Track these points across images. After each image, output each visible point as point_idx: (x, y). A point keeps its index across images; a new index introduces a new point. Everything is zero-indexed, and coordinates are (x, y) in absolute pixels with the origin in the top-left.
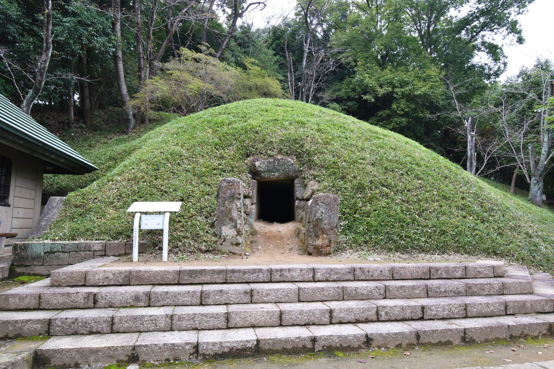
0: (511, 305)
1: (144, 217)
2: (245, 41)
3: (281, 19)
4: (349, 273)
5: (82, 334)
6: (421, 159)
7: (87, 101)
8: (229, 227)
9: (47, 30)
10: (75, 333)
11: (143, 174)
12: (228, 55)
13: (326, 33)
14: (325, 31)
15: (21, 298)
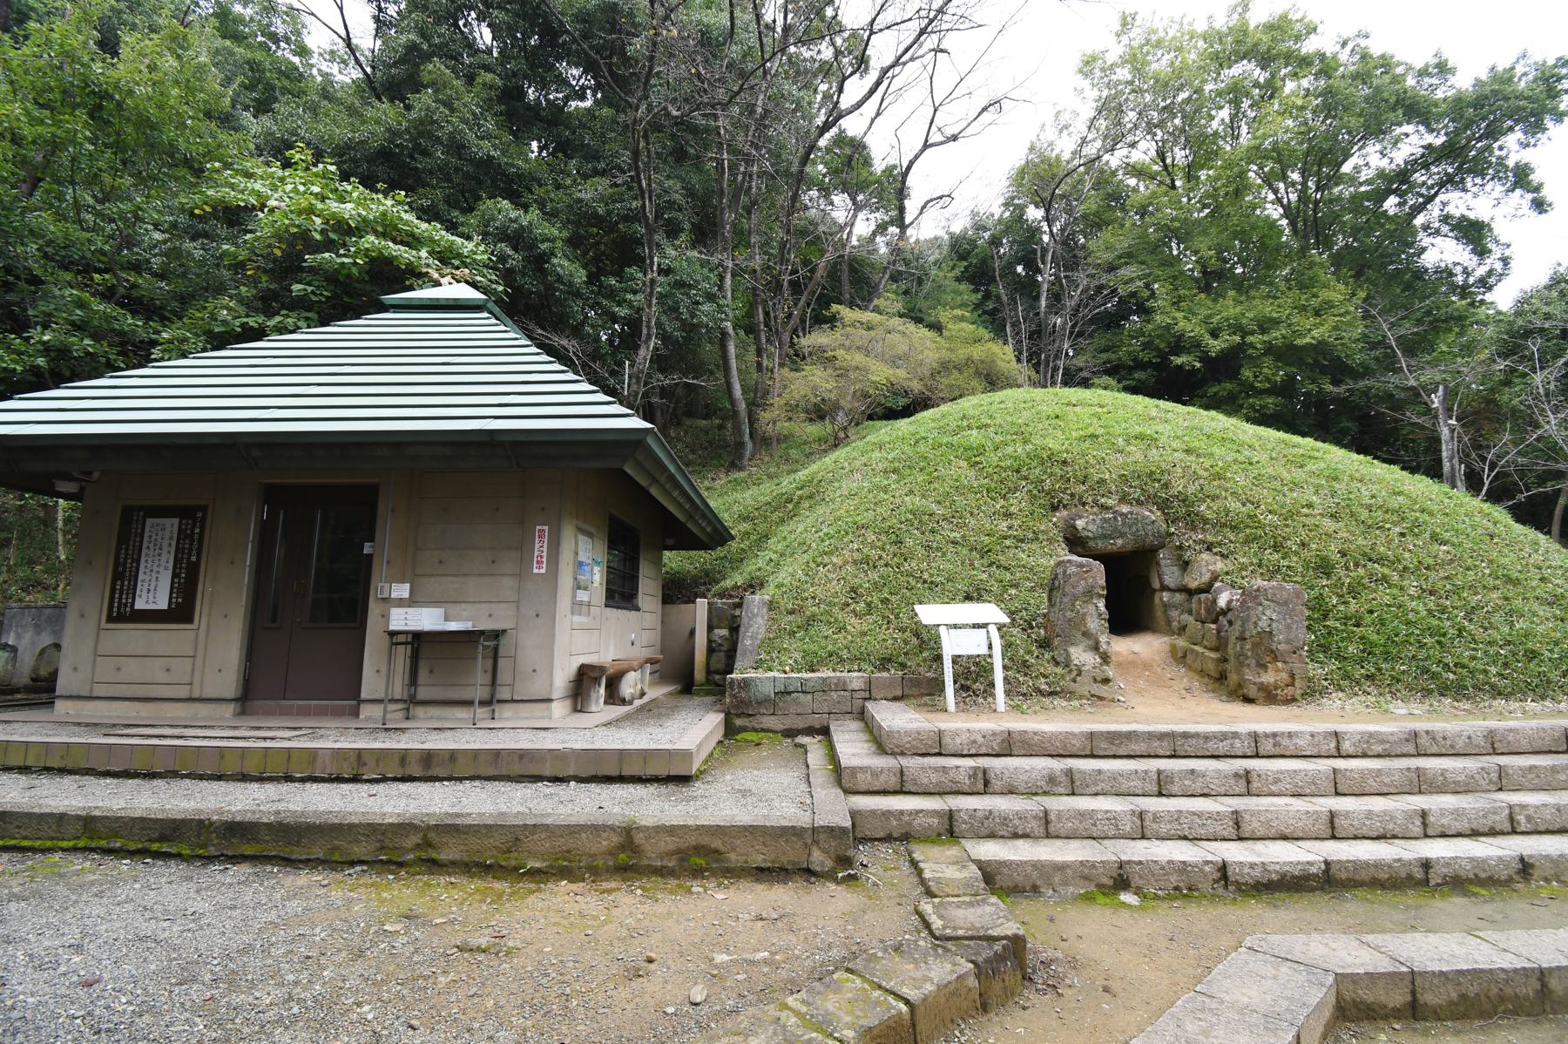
2: (908, 274)
5: (1002, 837)
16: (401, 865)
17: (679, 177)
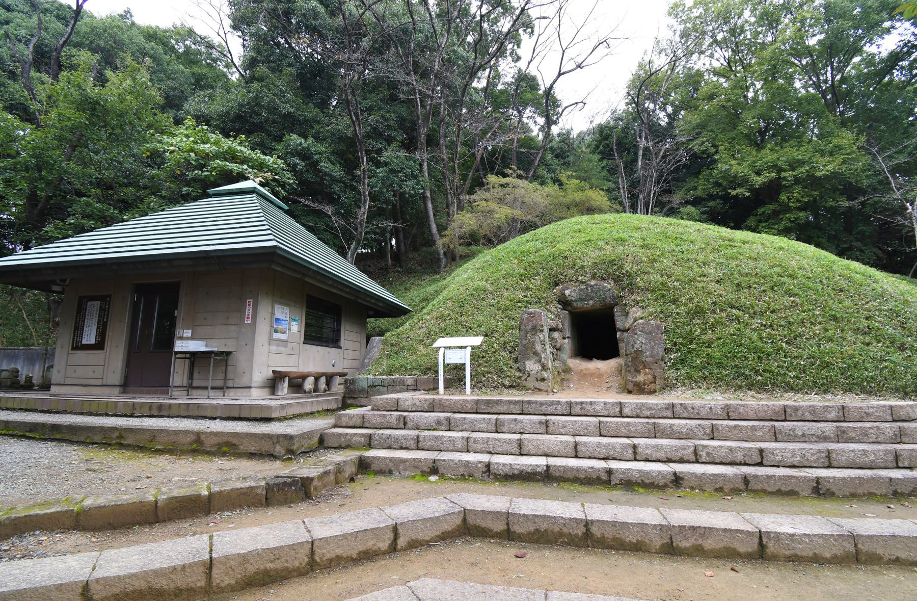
0: (905, 454)
1: (447, 351)
2: (564, 151)
3: (609, 113)
4: (667, 409)
6: (800, 268)
7: (402, 245)
8: (533, 361)
9: (364, 184)
10: (389, 448)
11: (450, 312)
12: (542, 171)
13: (672, 118)
14: (669, 116)
15: (351, 417)
16: (110, 445)
17: (395, 112)
